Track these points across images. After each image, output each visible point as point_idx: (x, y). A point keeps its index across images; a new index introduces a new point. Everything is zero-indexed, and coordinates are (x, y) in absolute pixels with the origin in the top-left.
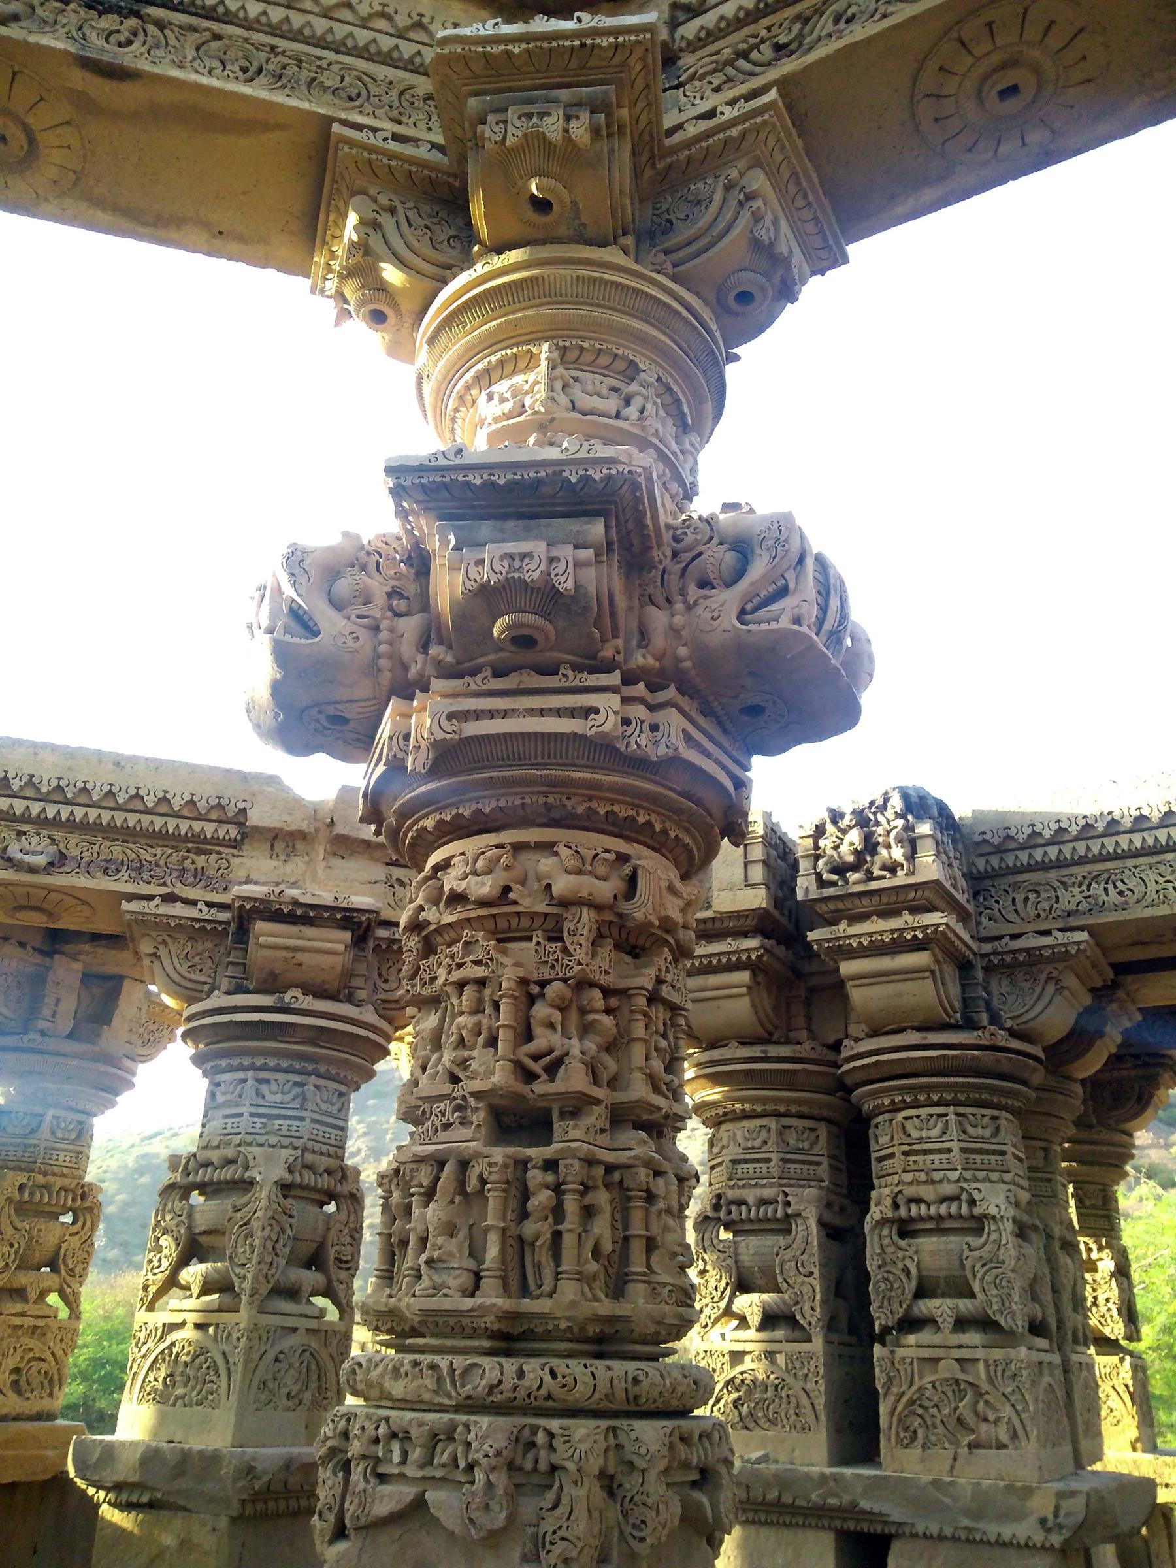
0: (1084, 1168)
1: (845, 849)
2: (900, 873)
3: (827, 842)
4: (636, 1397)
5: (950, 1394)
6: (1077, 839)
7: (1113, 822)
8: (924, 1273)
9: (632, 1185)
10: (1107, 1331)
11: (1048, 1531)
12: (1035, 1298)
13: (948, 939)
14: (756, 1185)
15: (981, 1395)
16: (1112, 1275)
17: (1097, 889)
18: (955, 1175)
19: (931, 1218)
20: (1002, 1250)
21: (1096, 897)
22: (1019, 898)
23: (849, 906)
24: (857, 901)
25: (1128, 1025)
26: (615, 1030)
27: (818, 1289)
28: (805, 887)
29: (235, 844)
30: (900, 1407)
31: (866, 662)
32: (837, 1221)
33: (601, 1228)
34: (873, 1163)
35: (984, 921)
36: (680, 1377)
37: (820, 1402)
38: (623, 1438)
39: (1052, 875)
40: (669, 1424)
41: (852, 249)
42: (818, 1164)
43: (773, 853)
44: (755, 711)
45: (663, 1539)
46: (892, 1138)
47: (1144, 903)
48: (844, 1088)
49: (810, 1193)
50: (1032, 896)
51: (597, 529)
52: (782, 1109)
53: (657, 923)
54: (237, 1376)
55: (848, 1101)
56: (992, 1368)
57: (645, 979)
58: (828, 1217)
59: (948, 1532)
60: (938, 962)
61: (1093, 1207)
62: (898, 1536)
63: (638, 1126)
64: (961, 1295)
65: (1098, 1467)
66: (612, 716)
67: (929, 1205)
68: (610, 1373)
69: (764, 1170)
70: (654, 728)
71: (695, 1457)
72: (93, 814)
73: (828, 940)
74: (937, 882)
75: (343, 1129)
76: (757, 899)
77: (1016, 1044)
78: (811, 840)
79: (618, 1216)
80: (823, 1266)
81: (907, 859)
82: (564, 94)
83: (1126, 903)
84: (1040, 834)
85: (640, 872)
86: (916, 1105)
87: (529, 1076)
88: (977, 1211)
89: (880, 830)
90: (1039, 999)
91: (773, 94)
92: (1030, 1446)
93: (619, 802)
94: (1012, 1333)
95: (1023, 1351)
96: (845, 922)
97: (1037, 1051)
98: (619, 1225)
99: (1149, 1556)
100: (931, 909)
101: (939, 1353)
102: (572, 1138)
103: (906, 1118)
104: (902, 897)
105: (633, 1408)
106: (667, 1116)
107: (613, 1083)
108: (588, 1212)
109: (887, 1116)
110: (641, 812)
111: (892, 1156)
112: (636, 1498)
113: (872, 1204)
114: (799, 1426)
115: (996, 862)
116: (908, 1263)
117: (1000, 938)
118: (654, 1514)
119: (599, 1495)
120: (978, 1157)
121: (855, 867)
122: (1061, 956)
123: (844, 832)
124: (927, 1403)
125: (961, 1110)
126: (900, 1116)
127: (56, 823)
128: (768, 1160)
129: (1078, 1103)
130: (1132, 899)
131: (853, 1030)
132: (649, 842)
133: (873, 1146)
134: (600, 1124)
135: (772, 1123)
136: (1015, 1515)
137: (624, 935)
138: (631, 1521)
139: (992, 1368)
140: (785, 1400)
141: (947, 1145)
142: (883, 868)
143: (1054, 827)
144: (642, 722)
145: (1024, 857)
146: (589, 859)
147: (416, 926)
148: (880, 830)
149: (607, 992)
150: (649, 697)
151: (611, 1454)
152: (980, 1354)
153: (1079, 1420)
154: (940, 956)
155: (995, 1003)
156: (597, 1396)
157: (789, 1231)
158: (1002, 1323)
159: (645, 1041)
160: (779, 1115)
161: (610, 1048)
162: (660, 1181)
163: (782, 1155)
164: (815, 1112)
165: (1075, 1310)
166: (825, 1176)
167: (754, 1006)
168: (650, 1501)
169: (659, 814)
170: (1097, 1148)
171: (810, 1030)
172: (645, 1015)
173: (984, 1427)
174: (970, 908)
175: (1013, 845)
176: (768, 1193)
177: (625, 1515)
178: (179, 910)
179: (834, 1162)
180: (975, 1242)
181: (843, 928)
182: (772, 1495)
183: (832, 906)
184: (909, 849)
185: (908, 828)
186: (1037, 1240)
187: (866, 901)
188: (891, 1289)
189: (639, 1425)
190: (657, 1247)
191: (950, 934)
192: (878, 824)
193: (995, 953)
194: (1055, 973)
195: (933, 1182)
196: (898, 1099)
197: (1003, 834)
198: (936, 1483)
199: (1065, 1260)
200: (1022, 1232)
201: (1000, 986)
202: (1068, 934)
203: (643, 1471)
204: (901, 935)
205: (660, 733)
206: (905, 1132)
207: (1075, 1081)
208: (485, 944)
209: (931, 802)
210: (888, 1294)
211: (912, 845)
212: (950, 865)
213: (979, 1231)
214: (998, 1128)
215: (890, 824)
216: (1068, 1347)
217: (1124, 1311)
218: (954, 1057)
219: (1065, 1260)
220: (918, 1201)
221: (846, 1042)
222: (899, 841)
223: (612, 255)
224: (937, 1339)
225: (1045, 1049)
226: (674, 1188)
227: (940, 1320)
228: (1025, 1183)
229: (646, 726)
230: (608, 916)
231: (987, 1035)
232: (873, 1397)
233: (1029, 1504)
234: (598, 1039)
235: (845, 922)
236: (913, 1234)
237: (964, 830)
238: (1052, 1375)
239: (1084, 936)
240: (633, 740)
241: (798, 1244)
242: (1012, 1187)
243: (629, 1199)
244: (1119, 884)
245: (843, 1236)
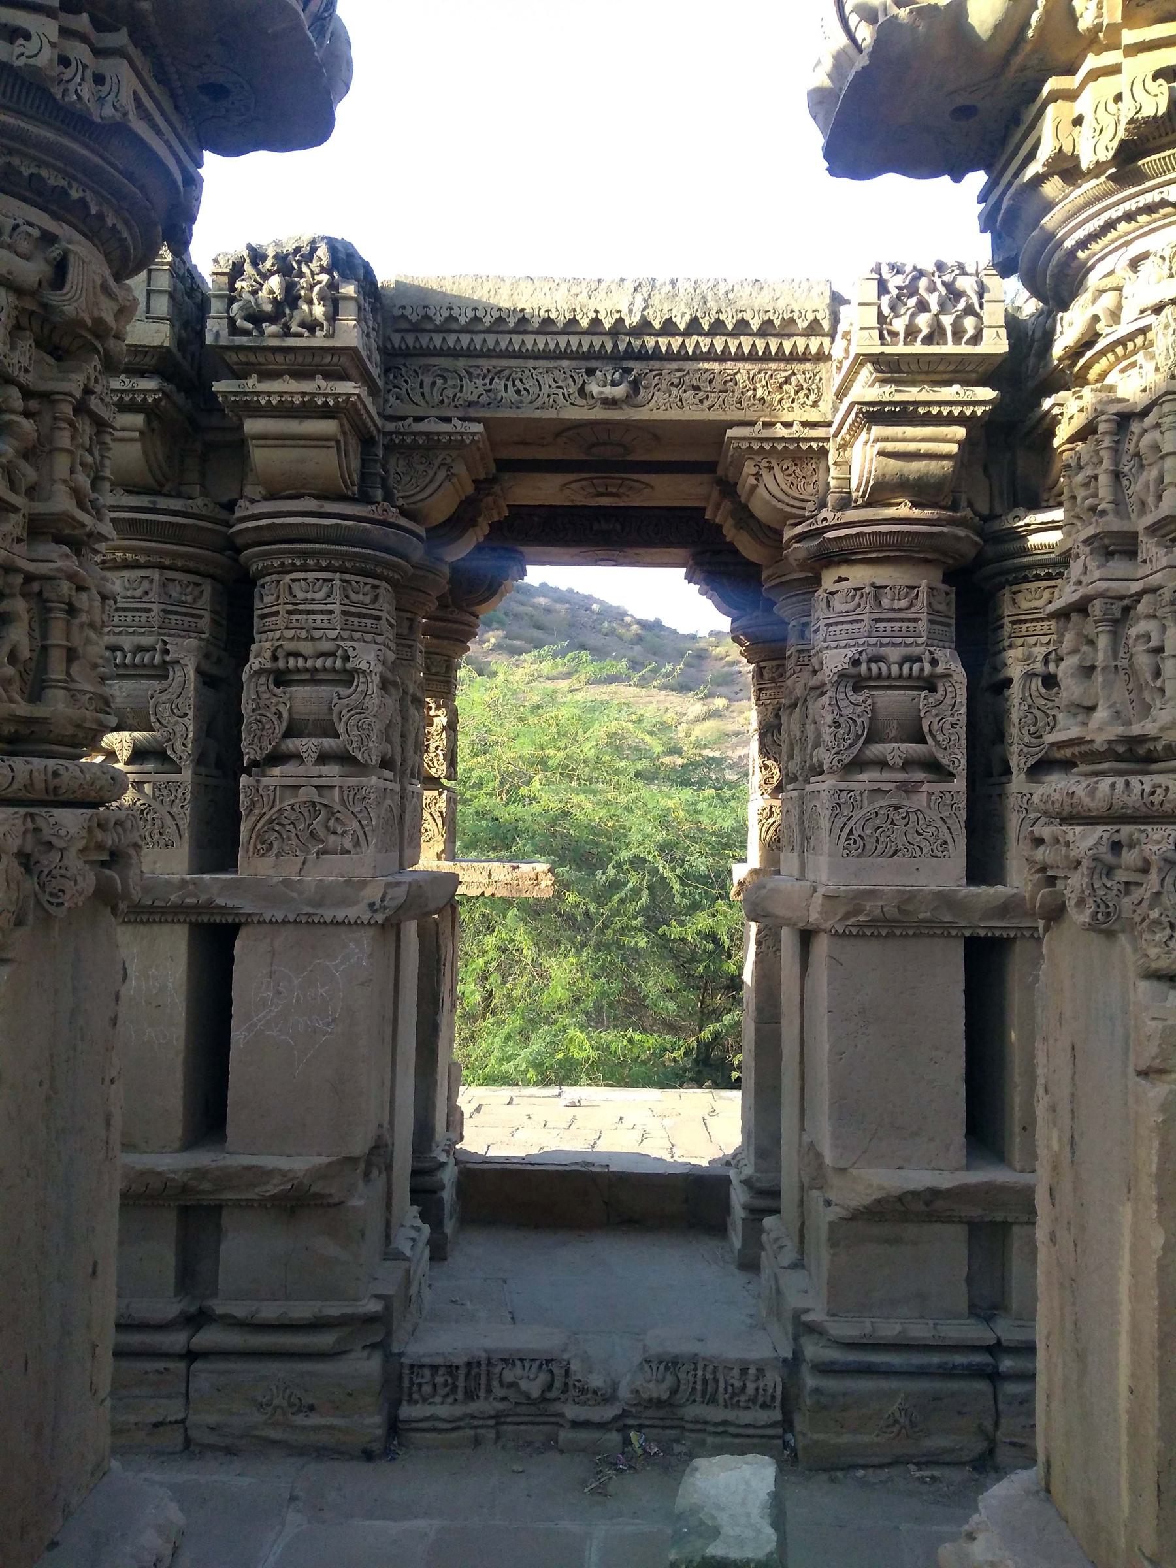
0: (435, 641)
1: (263, 294)
2: (318, 333)
3: (244, 284)
4: (56, 788)
5: (306, 814)
6: (488, 331)
7: (524, 320)
8: (295, 716)
9: (53, 596)
10: (433, 771)
11: (375, 911)
12: (388, 740)
13: (357, 411)
14: (134, 633)
15: (333, 814)
16: (444, 728)
17: (498, 384)
18: (333, 634)
19: (307, 670)
20: (368, 698)
21: (496, 392)
22: (428, 380)
23: (261, 360)
24: (270, 357)
25: (496, 518)
26: (35, 435)
27: (191, 728)
28: (215, 330)
30: (259, 825)
31: (344, 67)
32: (214, 671)
34: (256, 619)
35: (392, 400)
36: (99, 773)
37: (185, 825)
38: (40, 822)
39: (461, 363)
40: (90, 812)
42: (200, 617)
43: (180, 286)
44: (217, 92)
45: (80, 904)
46: (278, 597)
47: (536, 404)
48: (233, 547)
49: (191, 642)
50: (439, 382)
52: (167, 562)
53: (89, 323)
55: (236, 561)
56: (346, 793)
57: (74, 384)
58: (206, 667)
59: (291, 918)
60: (344, 433)
61: (436, 674)
62: (247, 923)
63: (58, 540)
64: (326, 736)
65: (416, 867)
66: (47, 48)
67: (306, 659)
68: (29, 767)
69: (144, 619)
70: (99, 79)
71: (109, 840)
73: (236, 394)
74: (355, 350)
77: (403, 522)
78: (226, 279)
79: (35, 626)
80: (198, 709)
81: (327, 319)
83: (521, 402)
84: (456, 319)
85: (71, 258)
86: (305, 569)
88: (349, 666)
89: (303, 282)
90: (430, 482)
92: (369, 853)
93: (48, 165)
94: (366, 766)
95: (374, 779)
96: (254, 377)
98: (37, 634)
99: (437, 933)
100: (344, 377)
101: (301, 781)
103: (293, 580)
104: (317, 360)
105: (51, 798)
106: (90, 535)
109: (274, 577)
110: (75, 184)
111: (276, 613)
112: (54, 872)
113: (252, 656)
114: (162, 842)
115: (417, 336)
116: (281, 708)
117: (404, 418)
118: (72, 883)
119: (17, 870)
120: (356, 620)
121: (272, 319)
122: (456, 444)
123: (266, 276)
124: (285, 822)
125: (346, 577)
126: (288, 578)
128: (149, 610)
129: (444, 582)
130: (526, 399)
131: (249, 490)
132: (81, 226)
133: (257, 604)
134: (18, 532)
135: (156, 575)
136: (345, 902)
137: (46, 331)
138: (48, 890)
139: (346, 793)
140: (150, 822)
141: (329, 607)
142: (302, 324)
143: (470, 314)
144: (85, 67)
145: (437, 340)
146: (8, 229)
148: (303, 282)
150: (93, 35)
151: (29, 836)
152: (336, 782)
153: (407, 834)
154: (347, 427)
155: (391, 482)
156: (15, 786)
157: (166, 677)
158: (359, 757)
159: (70, 452)
160: (163, 567)
161: (27, 454)
162: (84, 596)
163: (163, 606)
164: (202, 568)
165: (415, 753)
166: (206, 629)
167: (145, 453)
168: (68, 874)
169: (96, 193)
170: (450, 625)
171: (202, 486)
172: (72, 424)
173: (332, 838)
174: (380, 383)
175: (429, 326)
176: (146, 641)
177: (42, 886)
179: (217, 618)
180: (344, 691)
181: (252, 383)
183: (242, 358)
184: (331, 309)
185: (333, 286)
186: (396, 694)
187: (279, 358)
188: (263, 729)
189: (60, 814)
190: (78, 658)
191: (360, 406)
192: (301, 275)
193: (398, 433)
194: (449, 460)
195: (313, 639)
196: (288, 561)
197: (422, 312)
198: (286, 883)
199: (412, 710)
200: (385, 685)
201: (396, 465)
203: (61, 850)
204: (311, 400)
205: (106, 89)
206: (291, 593)
207: (446, 563)
209: (357, 261)
210: (259, 733)
211: (334, 304)
212: (368, 335)
213: (349, 683)
214: (377, 596)
215: (315, 277)
216: (406, 781)
217: (449, 757)
218: (346, 526)
219: (412, 710)
220: (297, 655)
221: (241, 502)
222: (322, 298)
224: (301, 770)
225: (428, 531)
226: (97, 604)
227: (304, 755)
228: (393, 645)
229: (89, 74)
230: (30, 305)
231: (380, 511)
232: (236, 818)
233: (362, 894)
234: (14, 442)
235: (254, 377)
236: (288, 683)
237: (383, 299)
238: (392, 800)
239: (479, 428)
240: (72, 87)
241: (175, 688)
242: (382, 648)
243: (50, 610)
244: (517, 382)
245: (221, 684)
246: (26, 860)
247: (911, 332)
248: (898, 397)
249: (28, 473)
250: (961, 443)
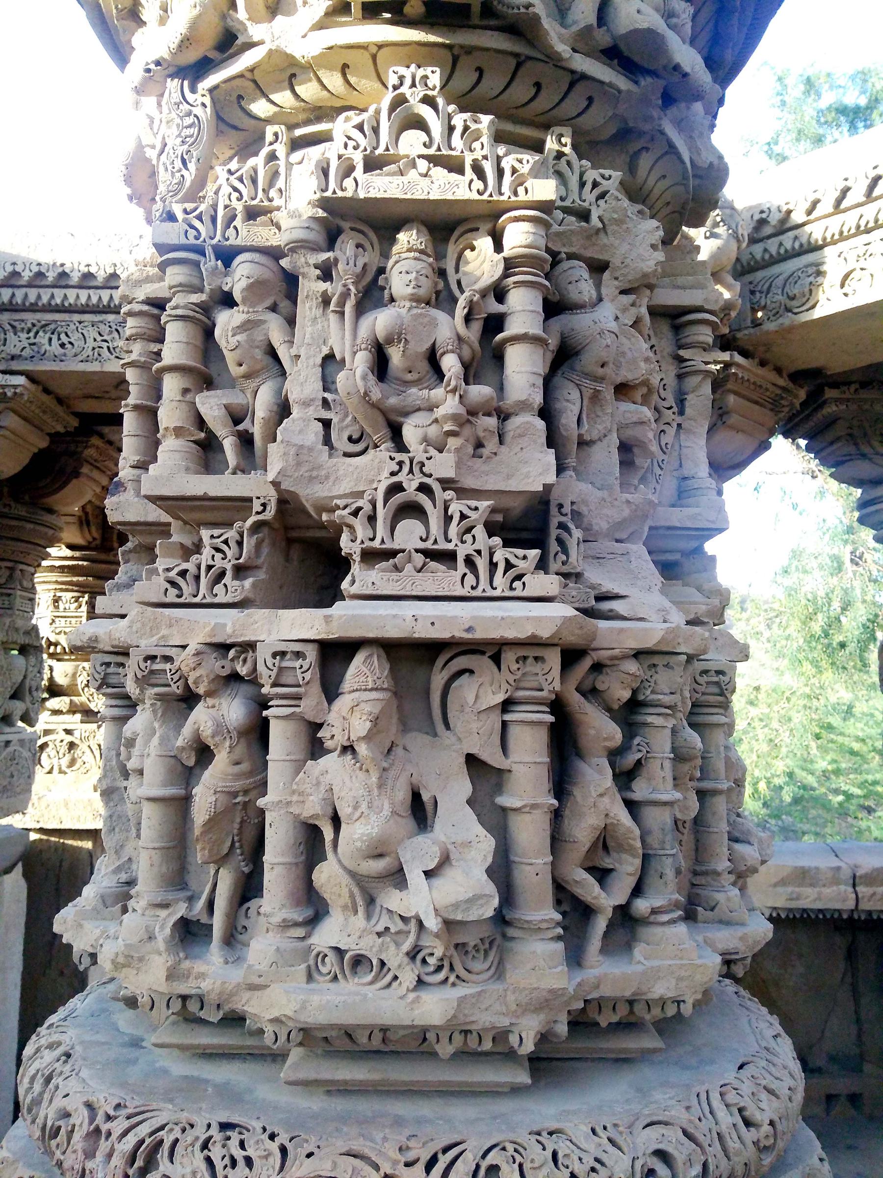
7: (64, 275)
17: (43, 338)
47: (80, 358)
75: (32, 600)
83: (65, 355)
202: (7, 376)
239: (21, 380)
244: (63, 336)
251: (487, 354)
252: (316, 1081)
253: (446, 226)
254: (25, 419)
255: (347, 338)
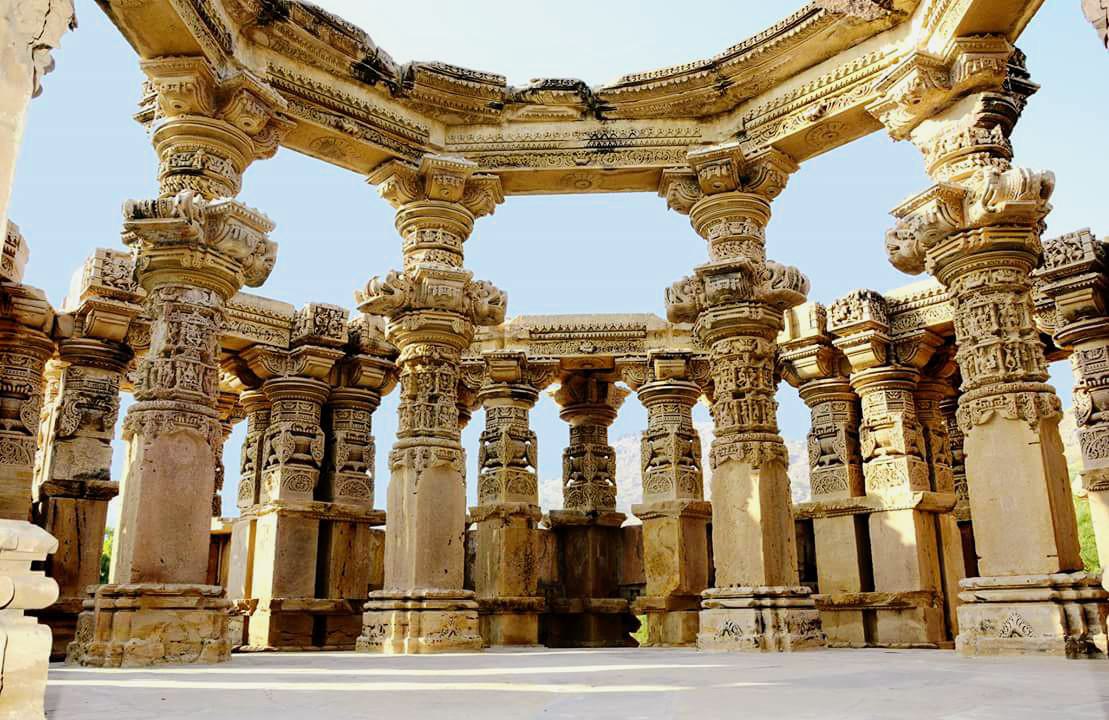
29: (645, 337)
33: (756, 412)
37: (848, 481)
39: (914, 312)
41: (800, 164)
51: (739, 275)
54: (674, 481)
58: (849, 430)
72: (594, 334)
76: (815, 332)
82: (719, 162)
87: (739, 386)
91: (770, 148)
97: (916, 370)
102: (748, 397)
107: (757, 386)
108: (754, 410)
121: (845, 319)
127: (591, 338)
147: (712, 360)
149: (754, 369)
178: (631, 359)
182: (833, 507)
208: (727, 363)
223: (736, 193)
246: (760, 450)
247: (1056, 263)
248: (1059, 285)
249: (756, 383)
250: (1093, 294)
251: (989, 319)
252: (863, 478)
253: (983, 307)
254: (988, 226)
255: (975, 320)
